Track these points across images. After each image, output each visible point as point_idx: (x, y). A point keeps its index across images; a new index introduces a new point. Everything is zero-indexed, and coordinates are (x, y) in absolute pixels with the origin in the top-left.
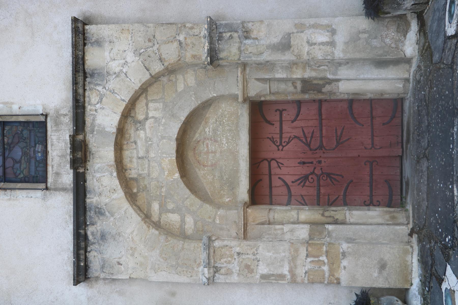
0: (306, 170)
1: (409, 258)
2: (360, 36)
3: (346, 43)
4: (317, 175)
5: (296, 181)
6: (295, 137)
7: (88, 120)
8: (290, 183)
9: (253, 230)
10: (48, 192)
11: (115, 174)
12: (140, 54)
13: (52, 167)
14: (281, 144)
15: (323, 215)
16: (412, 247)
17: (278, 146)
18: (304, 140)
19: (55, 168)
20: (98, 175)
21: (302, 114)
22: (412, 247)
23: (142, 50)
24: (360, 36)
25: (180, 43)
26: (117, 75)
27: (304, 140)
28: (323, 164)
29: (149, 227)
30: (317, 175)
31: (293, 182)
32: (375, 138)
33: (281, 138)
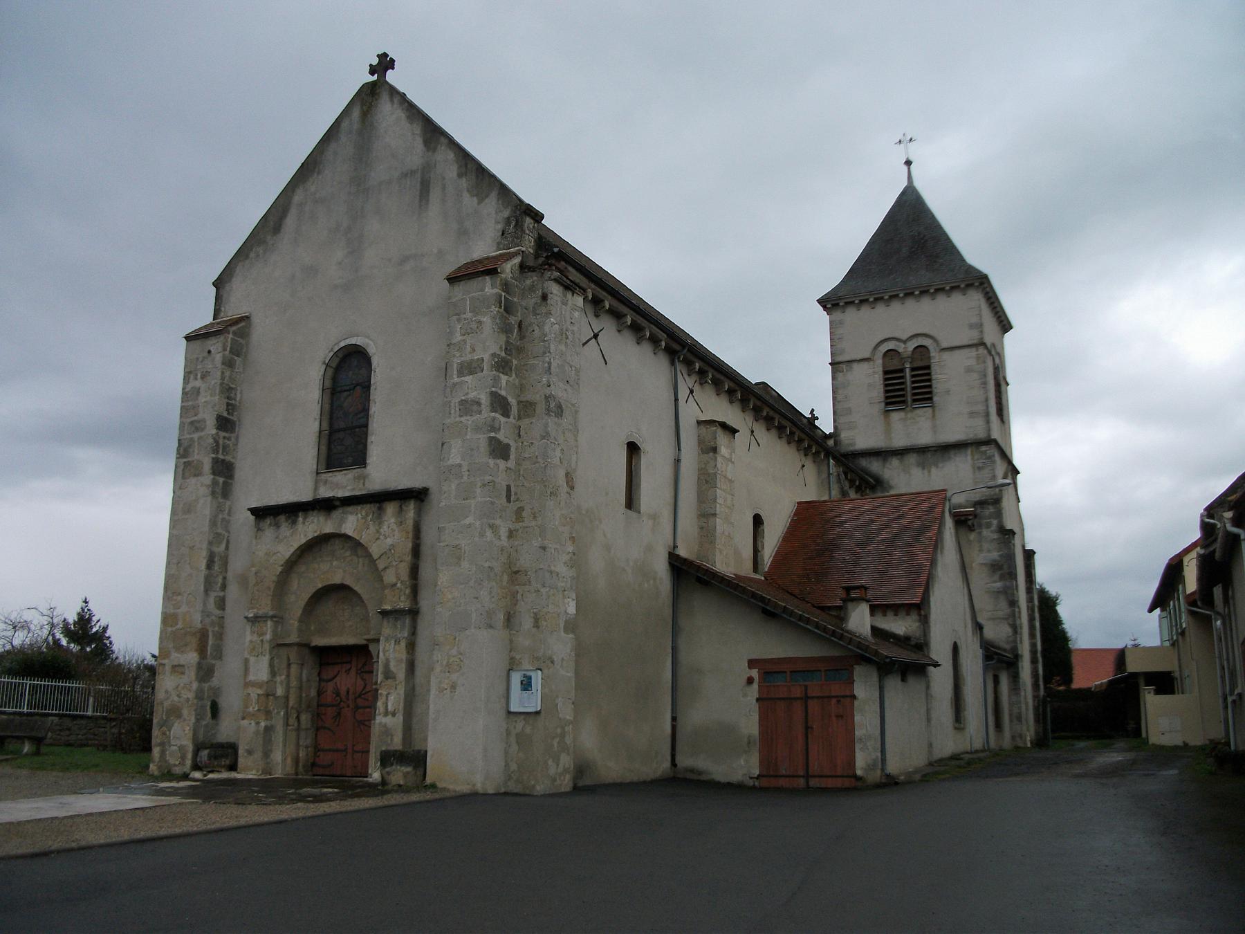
0: (343, 693)
1: (254, 772)
2: (390, 737)
3: (385, 726)
4: (339, 704)
5: (336, 686)
6: (366, 685)
7: (350, 509)
8: (335, 681)
9: (283, 652)
10: (315, 474)
11: (316, 535)
12: (390, 550)
13: (331, 476)
14: (362, 672)
15: (292, 708)
16: (261, 775)
17: (360, 669)
18: (363, 692)
19: (331, 479)
20: (315, 521)
21: (1221, 722)
22: (261, 775)
23: (393, 551)
24: (390, 737)
25: (395, 585)
26: (378, 532)
27: (363, 692)
28: (347, 709)
29: (282, 566)
30: (339, 704)
31: (336, 683)
32: (360, 754)
33: (366, 672)
